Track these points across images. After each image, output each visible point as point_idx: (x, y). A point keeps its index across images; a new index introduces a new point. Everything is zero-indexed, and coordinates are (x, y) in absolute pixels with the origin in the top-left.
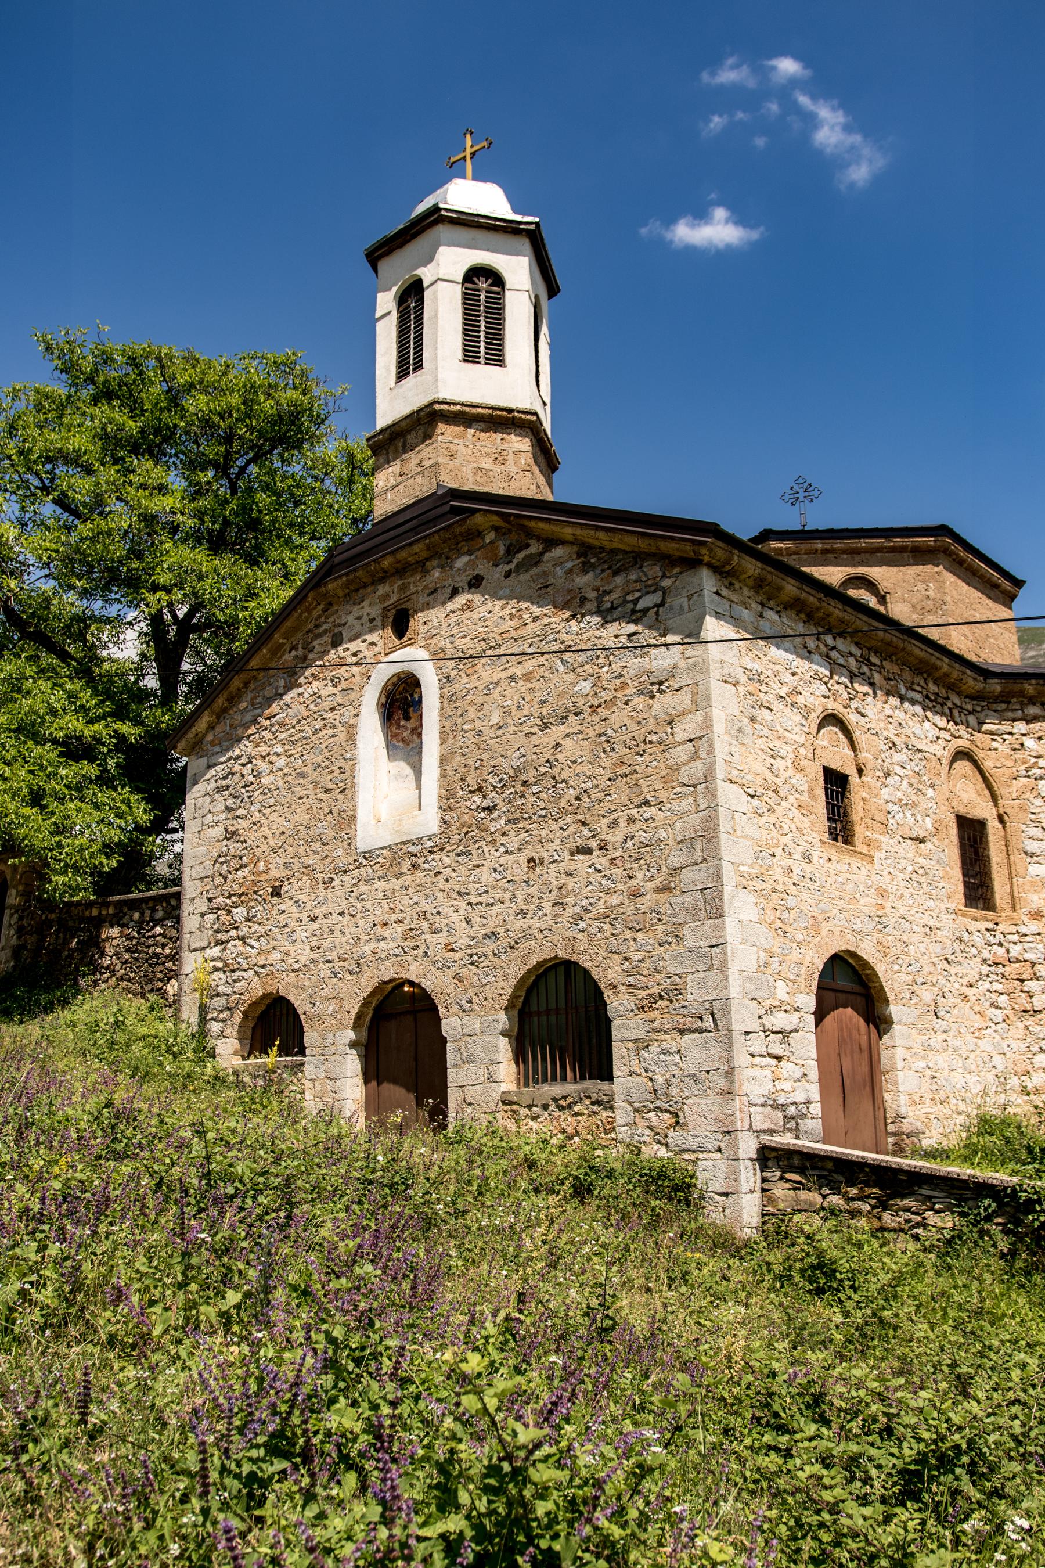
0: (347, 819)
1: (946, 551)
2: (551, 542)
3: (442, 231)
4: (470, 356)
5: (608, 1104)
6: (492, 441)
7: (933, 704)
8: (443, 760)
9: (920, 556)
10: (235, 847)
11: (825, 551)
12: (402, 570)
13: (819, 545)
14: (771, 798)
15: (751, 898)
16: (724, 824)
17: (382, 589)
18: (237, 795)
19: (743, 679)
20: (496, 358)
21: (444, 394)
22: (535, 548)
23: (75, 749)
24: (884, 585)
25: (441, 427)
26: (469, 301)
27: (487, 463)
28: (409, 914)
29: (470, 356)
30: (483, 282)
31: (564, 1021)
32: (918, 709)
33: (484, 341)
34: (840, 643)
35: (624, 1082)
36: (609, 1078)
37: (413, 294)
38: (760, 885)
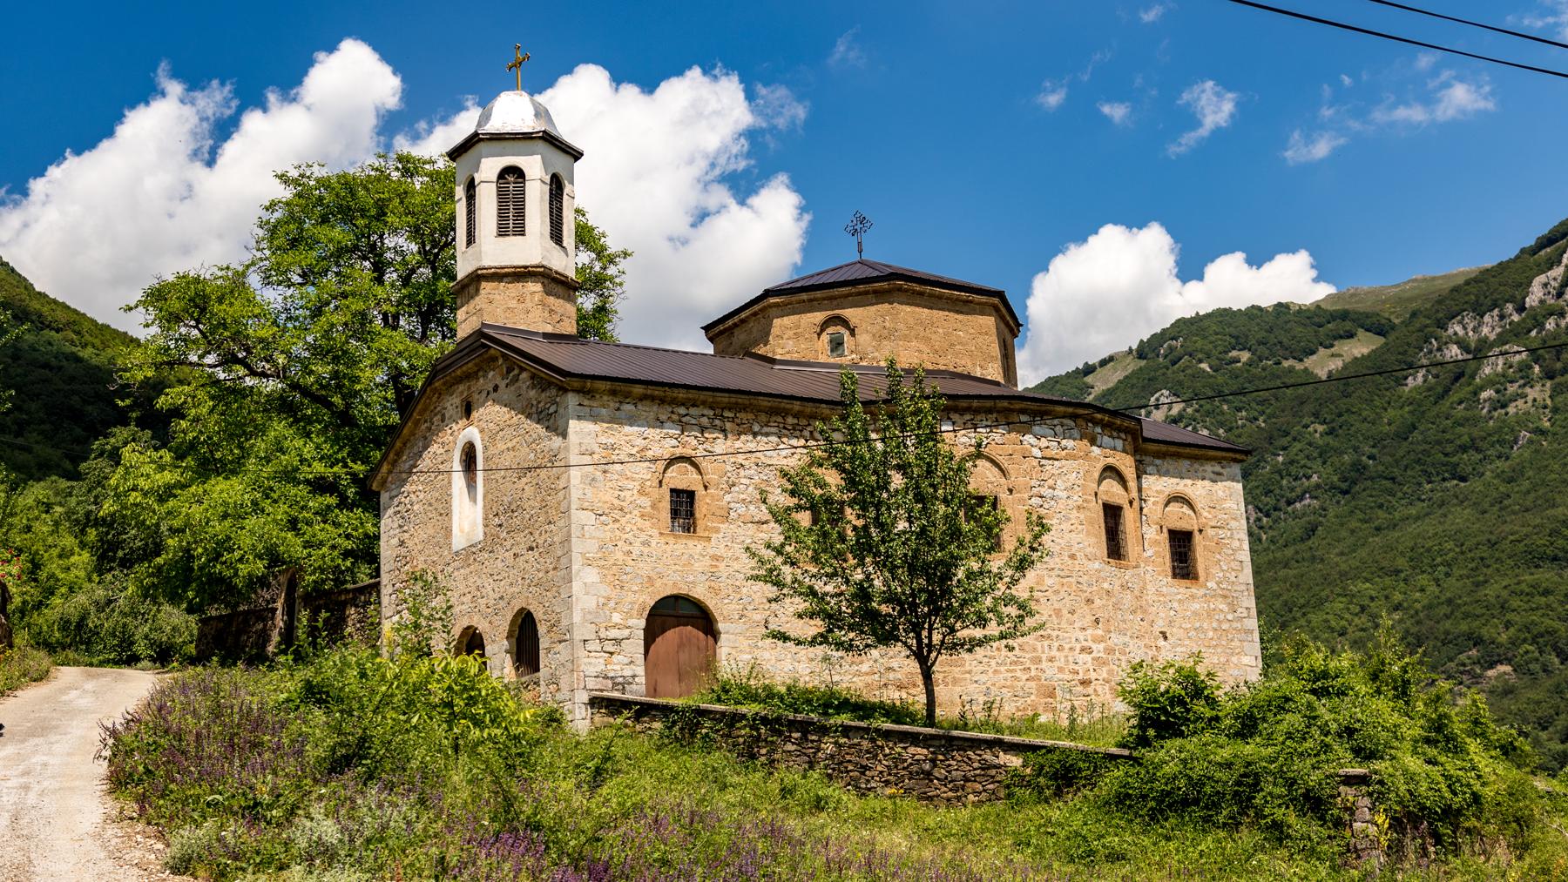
0: (448, 532)
1: (900, 289)
2: (522, 369)
3: (481, 147)
4: (502, 232)
5: (537, 683)
6: (515, 288)
7: (785, 431)
8: (485, 497)
9: (881, 296)
10: (403, 551)
11: (811, 300)
12: (468, 377)
13: (804, 296)
14: (617, 514)
15: (596, 570)
16: (575, 532)
17: (461, 387)
18: (404, 518)
19: (597, 450)
20: (521, 231)
21: (486, 263)
22: (516, 372)
23: (320, 486)
24: (853, 322)
25: (484, 284)
26: (502, 195)
27: (513, 304)
28: (473, 589)
29: (502, 232)
30: (512, 174)
31: (526, 641)
32: (774, 439)
33: (512, 221)
34: (693, 411)
35: (544, 672)
36: (538, 670)
37: (471, 187)
38: (602, 563)
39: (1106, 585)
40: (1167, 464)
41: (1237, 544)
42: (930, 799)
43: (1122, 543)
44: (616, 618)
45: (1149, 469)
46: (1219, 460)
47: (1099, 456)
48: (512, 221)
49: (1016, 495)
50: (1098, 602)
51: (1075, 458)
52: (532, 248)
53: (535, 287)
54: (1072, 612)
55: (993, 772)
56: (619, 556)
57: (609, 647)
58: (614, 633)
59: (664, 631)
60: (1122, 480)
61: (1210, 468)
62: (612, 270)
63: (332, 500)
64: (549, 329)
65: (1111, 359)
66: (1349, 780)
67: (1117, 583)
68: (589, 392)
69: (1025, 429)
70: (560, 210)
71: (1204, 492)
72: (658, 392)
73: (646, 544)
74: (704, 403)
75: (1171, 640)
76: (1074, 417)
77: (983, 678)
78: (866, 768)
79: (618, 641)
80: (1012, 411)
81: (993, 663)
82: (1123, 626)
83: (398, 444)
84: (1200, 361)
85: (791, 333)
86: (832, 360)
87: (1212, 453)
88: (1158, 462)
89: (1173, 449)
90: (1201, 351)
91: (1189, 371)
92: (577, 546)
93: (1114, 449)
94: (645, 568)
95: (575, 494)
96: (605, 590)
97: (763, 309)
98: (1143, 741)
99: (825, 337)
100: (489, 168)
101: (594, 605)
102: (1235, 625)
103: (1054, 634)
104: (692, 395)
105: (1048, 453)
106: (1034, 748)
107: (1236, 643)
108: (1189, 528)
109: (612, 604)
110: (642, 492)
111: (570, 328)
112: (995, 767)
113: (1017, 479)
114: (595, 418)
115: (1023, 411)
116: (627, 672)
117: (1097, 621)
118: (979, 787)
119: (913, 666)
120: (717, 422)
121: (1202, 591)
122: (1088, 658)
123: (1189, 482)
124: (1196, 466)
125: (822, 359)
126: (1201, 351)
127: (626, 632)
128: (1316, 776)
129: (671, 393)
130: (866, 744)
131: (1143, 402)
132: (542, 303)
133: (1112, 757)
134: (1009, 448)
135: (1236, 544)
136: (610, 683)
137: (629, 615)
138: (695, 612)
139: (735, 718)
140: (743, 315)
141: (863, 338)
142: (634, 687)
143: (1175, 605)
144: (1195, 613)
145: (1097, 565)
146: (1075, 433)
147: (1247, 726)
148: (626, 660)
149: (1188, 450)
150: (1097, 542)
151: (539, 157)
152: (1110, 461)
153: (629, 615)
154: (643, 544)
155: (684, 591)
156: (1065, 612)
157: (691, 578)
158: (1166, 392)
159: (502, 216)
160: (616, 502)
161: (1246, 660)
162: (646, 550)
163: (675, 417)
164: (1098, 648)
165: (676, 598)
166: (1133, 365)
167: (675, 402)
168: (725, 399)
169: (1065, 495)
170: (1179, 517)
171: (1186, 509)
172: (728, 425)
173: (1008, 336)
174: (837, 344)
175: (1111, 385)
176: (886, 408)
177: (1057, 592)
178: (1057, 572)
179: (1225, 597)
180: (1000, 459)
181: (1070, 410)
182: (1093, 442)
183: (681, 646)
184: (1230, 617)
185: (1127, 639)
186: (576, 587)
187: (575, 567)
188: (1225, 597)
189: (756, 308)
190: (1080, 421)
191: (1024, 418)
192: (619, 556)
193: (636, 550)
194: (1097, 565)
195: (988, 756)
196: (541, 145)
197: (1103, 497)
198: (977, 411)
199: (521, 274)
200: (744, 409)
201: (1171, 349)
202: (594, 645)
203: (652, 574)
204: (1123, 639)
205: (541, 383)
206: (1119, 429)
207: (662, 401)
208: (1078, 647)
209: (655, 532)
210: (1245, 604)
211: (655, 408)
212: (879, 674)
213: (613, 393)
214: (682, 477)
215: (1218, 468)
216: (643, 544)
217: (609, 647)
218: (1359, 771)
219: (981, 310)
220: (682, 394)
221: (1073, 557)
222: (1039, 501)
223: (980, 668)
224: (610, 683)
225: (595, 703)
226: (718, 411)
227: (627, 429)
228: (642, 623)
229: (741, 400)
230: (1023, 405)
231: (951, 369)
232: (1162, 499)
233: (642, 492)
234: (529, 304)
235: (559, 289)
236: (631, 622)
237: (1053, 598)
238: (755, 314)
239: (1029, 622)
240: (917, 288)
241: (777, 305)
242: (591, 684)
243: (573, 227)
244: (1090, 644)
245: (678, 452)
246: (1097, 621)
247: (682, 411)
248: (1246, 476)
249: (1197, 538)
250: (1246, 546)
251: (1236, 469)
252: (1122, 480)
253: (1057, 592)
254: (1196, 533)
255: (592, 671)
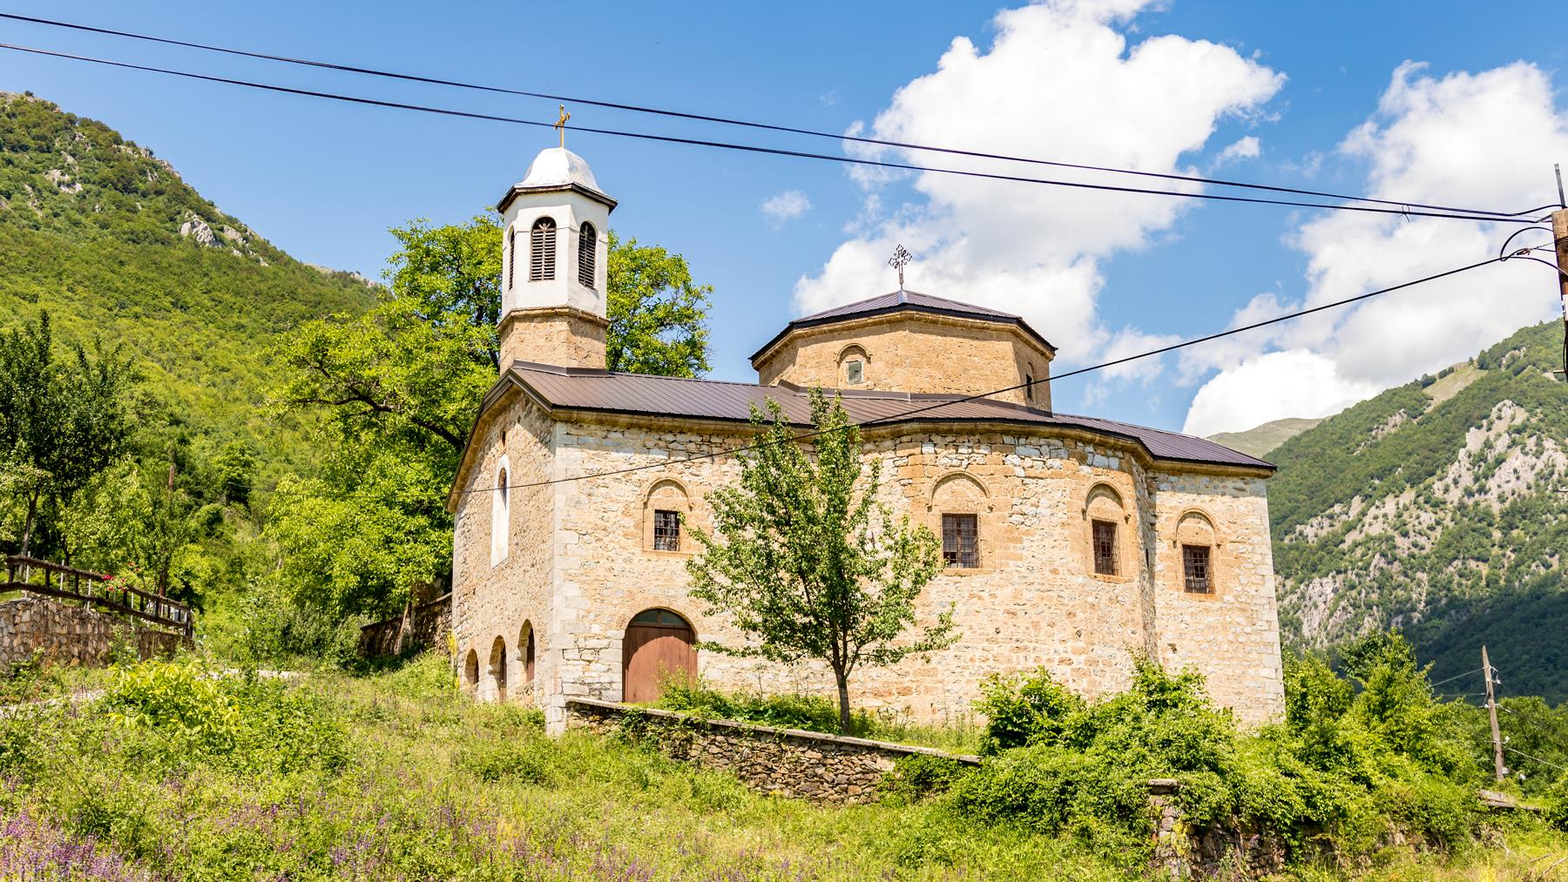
1: (912, 319)
4: (535, 277)
6: (544, 327)
9: (894, 325)
13: (825, 327)
14: (600, 534)
20: (550, 275)
21: (519, 306)
26: (536, 242)
27: (542, 342)
29: (535, 277)
33: (543, 267)
34: (680, 437)
39: (1091, 599)
40: (1182, 481)
41: (1259, 558)
42: (819, 800)
43: (1116, 558)
44: (596, 629)
45: (1162, 486)
46: (1241, 476)
47: (1089, 475)
48: (543, 267)
49: (995, 513)
50: (1080, 615)
51: (1060, 477)
52: (562, 289)
53: (561, 326)
54: (1052, 625)
55: (870, 776)
56: (601, 572)
57: (587, 655)
58: (592, 643)
59: (645, 642)
60: (1117, 497)
61: (1231, 483)
62: (699, 305)
63: (422, 520)
64: (574, 364)
65: (1451, 370)
66: (1156, 790)
67: (1104, 597)
68: (576, 422)
69: (1009, 450)
70: (592, 255)
71: (1223, 508)
72: (643, 420)
73: (628, 560)
74: (691, 430)
75: (1180, 651)
76: (1061, 437)
77: (956, 687)
78: (771, 769)
79: (596, 651)
80: (995, 432)
81: (966, 673)
82: (1108, 638)
83: (463, 471)
84: (1545, 370)
85: (812, 362)
86: (849, 387)
87: (1231, 469)
88: (1172, 478)
89: (1188, 466)
90: (1546, 360)
91: (1533, 381)
92: (559, 564)
93: (1109, 467)
94: (626, 583)
95: (559, 516)
96: (586, 603)
97: (791, 341)
98: (992, 751)
99: (844, 365)
100: (524, 216)
101: (574, 616)
102: (1253, 638)
103: (1031, 646)
104: (678, 422)
105: (1032, 472)
106: (905, 754)
107: (1254, 656)
108: (1205, 543)
109: (592, 616)
110: (626, 513)
111: (600, 362)
112: (872, 771)
113: (997, 495)
114: (581, 445)
115: (1006, 433)
116: (605, 679)
117: (1079, 634)
118: (859, 790)
119: (832, 675)
120: (704, 448)
121: (1218, 605)
122: (1068, 669)
123: (1207, 498)
124: (1216, 482)
125: (842, 386)
126: (1546, 360)
127: (605, 642)
128: (1128, 784)
129: (655, 421)
130: (773, 748)
131: (1485, 412)
132: (568, 341)
133: (966, 764)
134: (991, 468)
135: (1257, 558)
136: (587, 689)
137: (608, 626)
138: (678, 623)
139: (673, 721)
140: (777, 347)
141: (877, 365)
142: (611, 692)
143: (1187, 618)
144: (1209, 627)
145: (1080, 580)
146: (1063, 452)
147: (1086, 735)
148: (605, 668)
149: (1205, 467)
150: (1083, 554)
151: (568, 207)
152: (1103, 479)
153: (608, 626)
154: (625, 561)
155: (664, 604)
156: (1043, 624)
157: (672, 592)
158: (1508, 402)
159: (535, 261)
160: (600, 523)
161: (1265, 672)
162: (628, 567)
163: (662, 444)
164: (1079, 660)
165: (659, 610)
166: (1476, 375)
167: (660, 429)
168: (711, 425)
169: (1049, 512)
170: (1194, 533)
171: (1203, 524)
172: (716, 450)
173: (1037, 359)
174: (855, 372)
175: (1451, 396)
176: (807, 434)
177: (1035, 606)
178: (1036, 586)
179: (1243, 610)
180: (980, 479)
181: (1056, 430)
182: (1082, 460)
183: (662, 655)
184: (1248, 630)
185: (1114, 651)
186: (557, 601)
187: (556, 582)
188: (1243, 610)
189: (785, 339)
190: (1068, 441)
191: (1008, 440)
192: (601, 572)
193: (618, 567)
194: (1080, 580)
195: (867, 761)
196: (571, 195)
197: (1093, 513)
198: (959, 433)
199: (550, 315)
200: (732, 434)
201: (1514, 359)
202: (574, 654)
203: (633, 589)
204: (1108, 651)
205: (544, 416)
206: (1114, 448)
207: (650, 429)
208: (1057, 658)
209: (638, 550)
210: (1266, 618)
211: (643, 435)
212: (806, 678)
213: (601, 422)
214: (666, 499)
215: (1240, 484)
216: (625, 561)
217: (587, 655)
218: (1169, 780)
219: (999, 336)
220: (668, 422)
221: (1055, 572)
222: (1021, 518)
223: (953, 678)
224: (587, 689)
225: (570, 706)
226: (706, 438)
227: (614, 455)
228: (622, 634)
229: (727, 426)
230: (1006, 426)
231: (964, 393)
232: (1176, 515)
233: (626, 513)
234: (556, 342)
235: (588, 328)
236: (610, 633)
237: (1032, 611)
238: (785, 345)
239: (948, 635)
240: (930, 316)
241: (801, 336)
242: (568, 689)
243: (605, 270)
244: (1070, 655)
245: (664, 476)
246: (1079, 634)
247: (670, 437)
248: (1270, 493)
249: (1215, 553)
250: (1269, 560)
251: (1260, 484)
252: (1117, 497)
253: (1035, 606)
254: (1214, 549)
255: (569, 677)
